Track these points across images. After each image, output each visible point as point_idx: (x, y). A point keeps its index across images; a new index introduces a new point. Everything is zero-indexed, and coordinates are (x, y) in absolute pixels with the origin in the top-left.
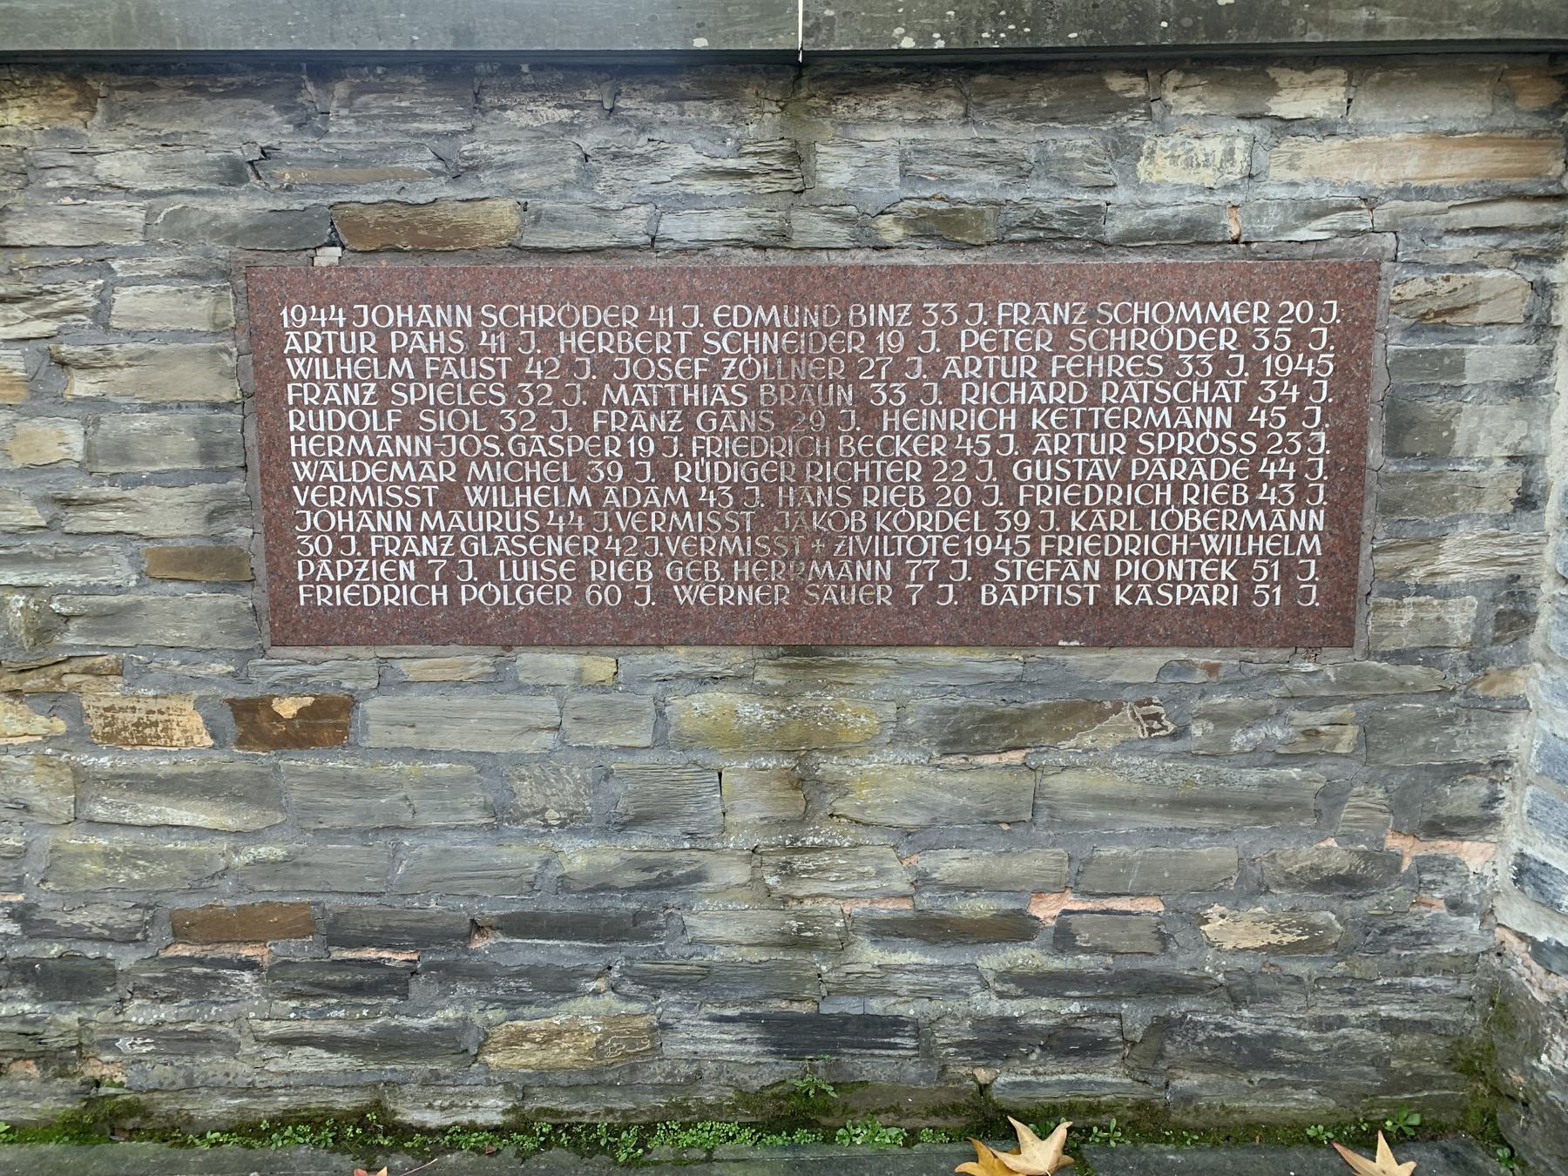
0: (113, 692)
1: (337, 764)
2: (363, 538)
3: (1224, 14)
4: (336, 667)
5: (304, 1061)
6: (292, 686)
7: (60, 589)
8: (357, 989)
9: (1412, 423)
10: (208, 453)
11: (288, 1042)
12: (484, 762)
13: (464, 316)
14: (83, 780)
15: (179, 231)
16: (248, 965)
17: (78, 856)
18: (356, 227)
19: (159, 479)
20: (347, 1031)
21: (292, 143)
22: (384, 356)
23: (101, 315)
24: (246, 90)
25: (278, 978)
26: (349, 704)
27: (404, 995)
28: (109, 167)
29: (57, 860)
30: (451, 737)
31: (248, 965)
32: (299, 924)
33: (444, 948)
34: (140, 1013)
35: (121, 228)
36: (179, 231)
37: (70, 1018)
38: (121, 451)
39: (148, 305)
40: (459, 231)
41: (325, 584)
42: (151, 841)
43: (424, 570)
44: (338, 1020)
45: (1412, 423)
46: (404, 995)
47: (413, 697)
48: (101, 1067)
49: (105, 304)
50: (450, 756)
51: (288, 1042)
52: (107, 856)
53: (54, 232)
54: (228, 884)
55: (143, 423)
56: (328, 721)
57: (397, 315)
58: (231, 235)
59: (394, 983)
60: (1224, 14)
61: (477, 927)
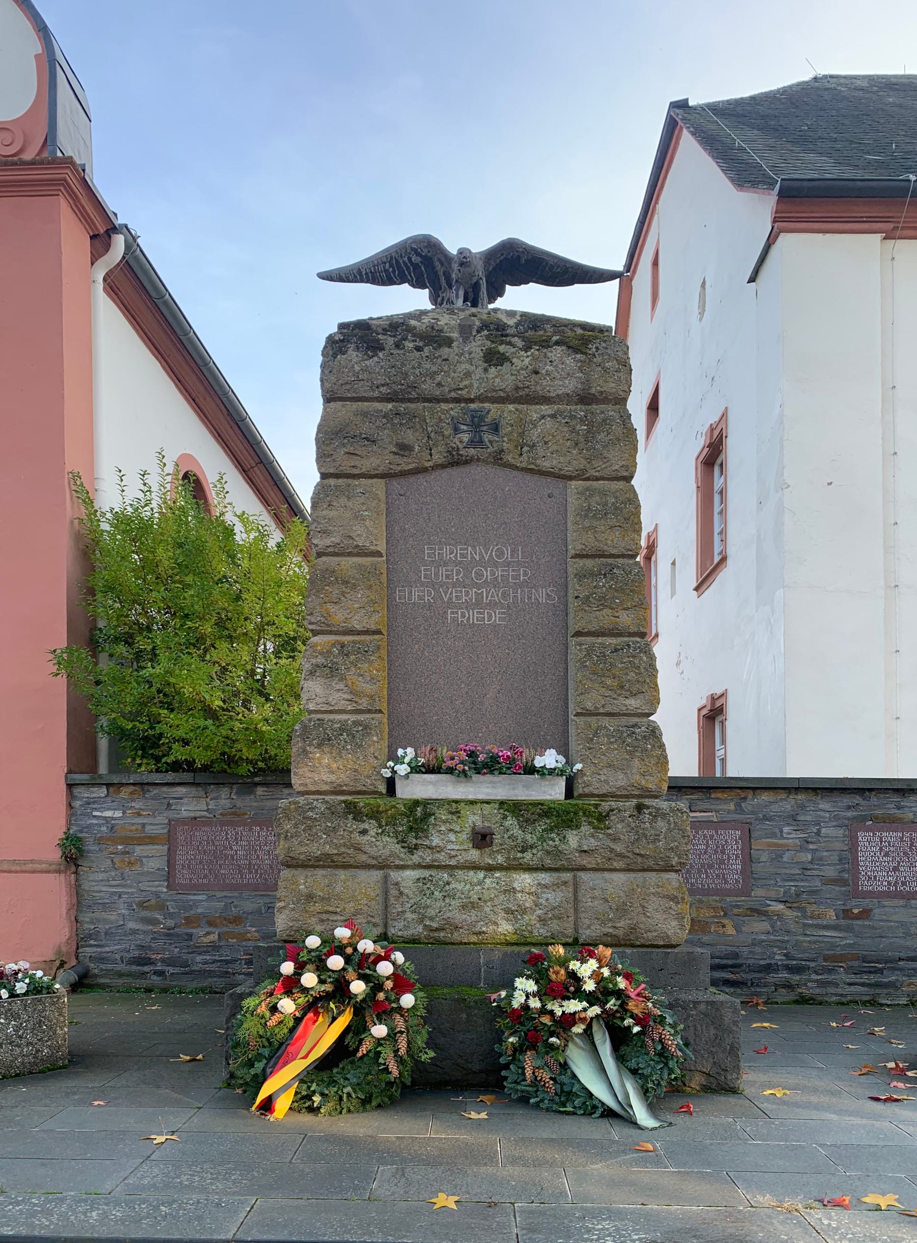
0: (814, 907)
1: (867, 923)
2: (875, 877)
3: (455, 266)
4: (866, 903)
5: (853, 989)
6: (857, 906)
7: (803, 886)
8: (870, 972)
9: (733, 1091)
10: (840, 860)
11: (850, 984)
12: (903, 924)
13: (900, 834)
14: (805, 925)
15: (836, 818)
16: (841, 967)
17: (802, 942)
18: (876, 818)
19: (829, 865)
20: (867, 981)
21: (863, 803)
22: (881, 842)
23: (818, 833)
24: (853, 793)
25: (850, 970)
26: (871, 910)
27: (882, 973)
28: (821, 806)
29: (797, 944)
30: (894, 918)
31: (841, 967)
32: (856, 957)
33: (892, 963)
34: (814, 977)
35: (824, 817)
36: (836, 818)
37: (798, 978)
38: (821, 859)
39: (828, 832)
40: (900, 819)
41: (865, 885)
42: (820, 939)
43: (889, 883)
44: (865, 978)
45: (733, 1091)
46: (882, 973)
47: (886, 909)
48: (803, 990)
49: (819, 831)
50: (895, 922)
51: (850, 984)
52: (809, 942)
53: (809, 818)
54: (839, 949)
55: (825, 854)
56: (866, 914)
57: (884, 834)
58: (849, 819)
59: (880, 971)
60: (455, 266)
61: (900, 959)
